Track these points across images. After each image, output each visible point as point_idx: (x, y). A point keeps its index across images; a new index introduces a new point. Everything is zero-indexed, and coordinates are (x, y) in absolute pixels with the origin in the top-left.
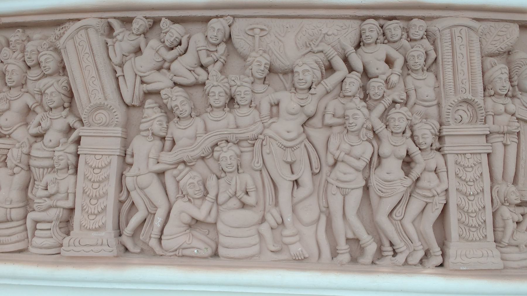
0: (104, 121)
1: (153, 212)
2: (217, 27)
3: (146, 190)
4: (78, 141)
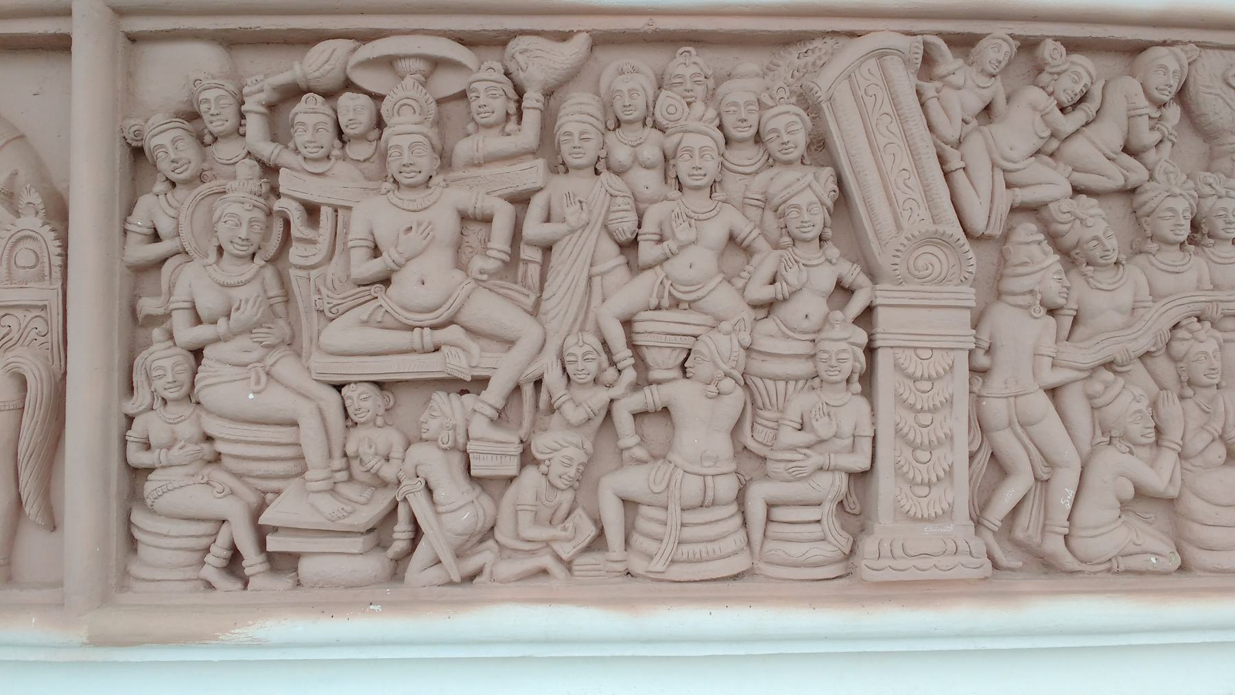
0: (937, 270)
1: (1045, 477)
2: (1165, 68)
3: (1031, 429)
4: (867, 316)
